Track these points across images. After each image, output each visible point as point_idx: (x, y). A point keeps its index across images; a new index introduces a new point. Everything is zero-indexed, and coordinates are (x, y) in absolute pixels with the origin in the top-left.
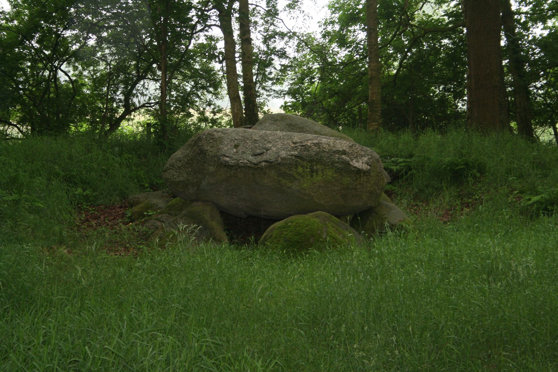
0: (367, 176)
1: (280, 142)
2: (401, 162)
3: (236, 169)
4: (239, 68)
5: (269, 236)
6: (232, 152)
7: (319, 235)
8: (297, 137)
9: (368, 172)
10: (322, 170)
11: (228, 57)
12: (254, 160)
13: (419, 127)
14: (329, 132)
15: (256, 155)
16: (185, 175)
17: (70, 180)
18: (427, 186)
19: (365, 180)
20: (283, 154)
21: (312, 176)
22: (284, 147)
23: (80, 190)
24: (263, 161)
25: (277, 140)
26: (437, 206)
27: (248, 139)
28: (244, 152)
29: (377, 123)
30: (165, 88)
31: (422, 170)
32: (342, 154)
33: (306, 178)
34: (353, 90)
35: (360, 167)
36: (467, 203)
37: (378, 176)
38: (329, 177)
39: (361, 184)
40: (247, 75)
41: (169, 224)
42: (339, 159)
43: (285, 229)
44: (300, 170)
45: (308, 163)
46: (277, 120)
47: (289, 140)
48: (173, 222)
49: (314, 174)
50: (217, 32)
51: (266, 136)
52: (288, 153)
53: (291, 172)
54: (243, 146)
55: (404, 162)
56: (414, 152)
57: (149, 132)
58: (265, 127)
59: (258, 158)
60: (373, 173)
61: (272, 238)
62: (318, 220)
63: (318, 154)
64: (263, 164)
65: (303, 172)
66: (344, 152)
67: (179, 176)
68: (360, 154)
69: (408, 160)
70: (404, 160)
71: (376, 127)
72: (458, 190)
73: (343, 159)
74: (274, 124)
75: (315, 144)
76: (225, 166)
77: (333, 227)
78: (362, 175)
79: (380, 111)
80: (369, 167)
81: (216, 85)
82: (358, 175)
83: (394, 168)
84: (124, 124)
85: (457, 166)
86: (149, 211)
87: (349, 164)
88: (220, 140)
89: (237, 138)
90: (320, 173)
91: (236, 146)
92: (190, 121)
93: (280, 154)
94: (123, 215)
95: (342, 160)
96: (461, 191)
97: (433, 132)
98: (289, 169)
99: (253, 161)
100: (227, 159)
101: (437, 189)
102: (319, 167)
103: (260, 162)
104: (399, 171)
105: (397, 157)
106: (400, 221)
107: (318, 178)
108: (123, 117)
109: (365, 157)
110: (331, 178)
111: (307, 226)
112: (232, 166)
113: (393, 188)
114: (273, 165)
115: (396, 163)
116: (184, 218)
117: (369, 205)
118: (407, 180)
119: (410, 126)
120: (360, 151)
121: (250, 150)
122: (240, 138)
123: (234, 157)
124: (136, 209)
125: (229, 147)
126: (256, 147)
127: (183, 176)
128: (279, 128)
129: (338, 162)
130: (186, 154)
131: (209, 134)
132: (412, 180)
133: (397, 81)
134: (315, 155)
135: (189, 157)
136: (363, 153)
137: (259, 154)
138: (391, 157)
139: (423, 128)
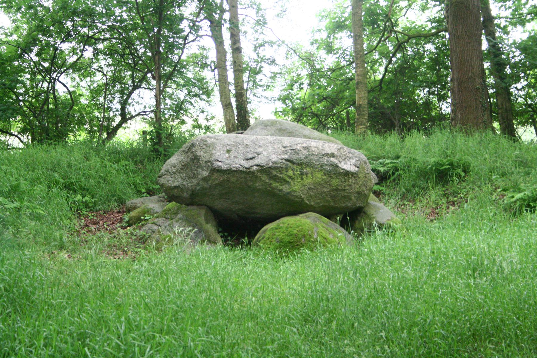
1: (270, 147)
2: (388, 164)
3: (229, 174)
4: (231, 76)
8: (287, 141)
10: (312, 173)
11: (220, 66)
12: (247, 164)
13: (404, 129)
15: (247, 160)
16: (180, 180)
17: (69, 187)
18: (414, 186)
19: (353, 182)
20: (274, 158)
21: (302, 179)
23: (79, 197)
25: (268, 145)
27: (240, 144)
28: (236, 157)
30: (159, 97)
31: (409, 171)
32: (330, 157)
35: (348, 169)
37: (366, 177)
40: (238, 82)
41: (165, 227)
42: (328, 161)
46: (268, 125)
48: (169, 225)
50: (209, 43)
51: (257, 140)
53: (281, 176)
55: (391, 163)
56: (400, 154)
57: (145, 139)
58: (256, 132)
61: (265, 239)
62: (309, 221)
65: (294, 175)
66: (333, 155)
67: (173, 182)
69: (395, 161)
70: (391, 161)
71: (363, 130)
74: (265, 129)
75: (305, 148)
76: (218, 171)
77: (324, 227)
78: (350, 176)
79: (367, 115)
80: (357, 169)
81: (208, 93)
82: (346, 176)
83: (382, 169)
84: (120, 131)
85: (443, 166)
86: (146, 215)
87: (337, 166)
88: (213, 145)
89: (229, 143)
90: (310, 175)
91: (228, 151)
92: (184, 128)
94: (122, 220)
100: (220, 164)
101: (423, 188)
102: (308, 169)
103: (252, 166)
105: (384, 158)
106: (388, 220)
107: (308, 181)
108: (119, 126)
109: (353, 159)
112: (225, 171)
113: (381, 188)
115: (384, 165)
116: (180, 221)
118: (394, 180)
122: (232, 143)
123: (227, 161)
124: (133, 214)
125: (222, 152)
126: (247, 152)
129: (326, 165)
132: (399, 180)
133: (383, 85)
136: (351, 155)
137: (251, 159)
138: (379, 158)
139: (409, 130)
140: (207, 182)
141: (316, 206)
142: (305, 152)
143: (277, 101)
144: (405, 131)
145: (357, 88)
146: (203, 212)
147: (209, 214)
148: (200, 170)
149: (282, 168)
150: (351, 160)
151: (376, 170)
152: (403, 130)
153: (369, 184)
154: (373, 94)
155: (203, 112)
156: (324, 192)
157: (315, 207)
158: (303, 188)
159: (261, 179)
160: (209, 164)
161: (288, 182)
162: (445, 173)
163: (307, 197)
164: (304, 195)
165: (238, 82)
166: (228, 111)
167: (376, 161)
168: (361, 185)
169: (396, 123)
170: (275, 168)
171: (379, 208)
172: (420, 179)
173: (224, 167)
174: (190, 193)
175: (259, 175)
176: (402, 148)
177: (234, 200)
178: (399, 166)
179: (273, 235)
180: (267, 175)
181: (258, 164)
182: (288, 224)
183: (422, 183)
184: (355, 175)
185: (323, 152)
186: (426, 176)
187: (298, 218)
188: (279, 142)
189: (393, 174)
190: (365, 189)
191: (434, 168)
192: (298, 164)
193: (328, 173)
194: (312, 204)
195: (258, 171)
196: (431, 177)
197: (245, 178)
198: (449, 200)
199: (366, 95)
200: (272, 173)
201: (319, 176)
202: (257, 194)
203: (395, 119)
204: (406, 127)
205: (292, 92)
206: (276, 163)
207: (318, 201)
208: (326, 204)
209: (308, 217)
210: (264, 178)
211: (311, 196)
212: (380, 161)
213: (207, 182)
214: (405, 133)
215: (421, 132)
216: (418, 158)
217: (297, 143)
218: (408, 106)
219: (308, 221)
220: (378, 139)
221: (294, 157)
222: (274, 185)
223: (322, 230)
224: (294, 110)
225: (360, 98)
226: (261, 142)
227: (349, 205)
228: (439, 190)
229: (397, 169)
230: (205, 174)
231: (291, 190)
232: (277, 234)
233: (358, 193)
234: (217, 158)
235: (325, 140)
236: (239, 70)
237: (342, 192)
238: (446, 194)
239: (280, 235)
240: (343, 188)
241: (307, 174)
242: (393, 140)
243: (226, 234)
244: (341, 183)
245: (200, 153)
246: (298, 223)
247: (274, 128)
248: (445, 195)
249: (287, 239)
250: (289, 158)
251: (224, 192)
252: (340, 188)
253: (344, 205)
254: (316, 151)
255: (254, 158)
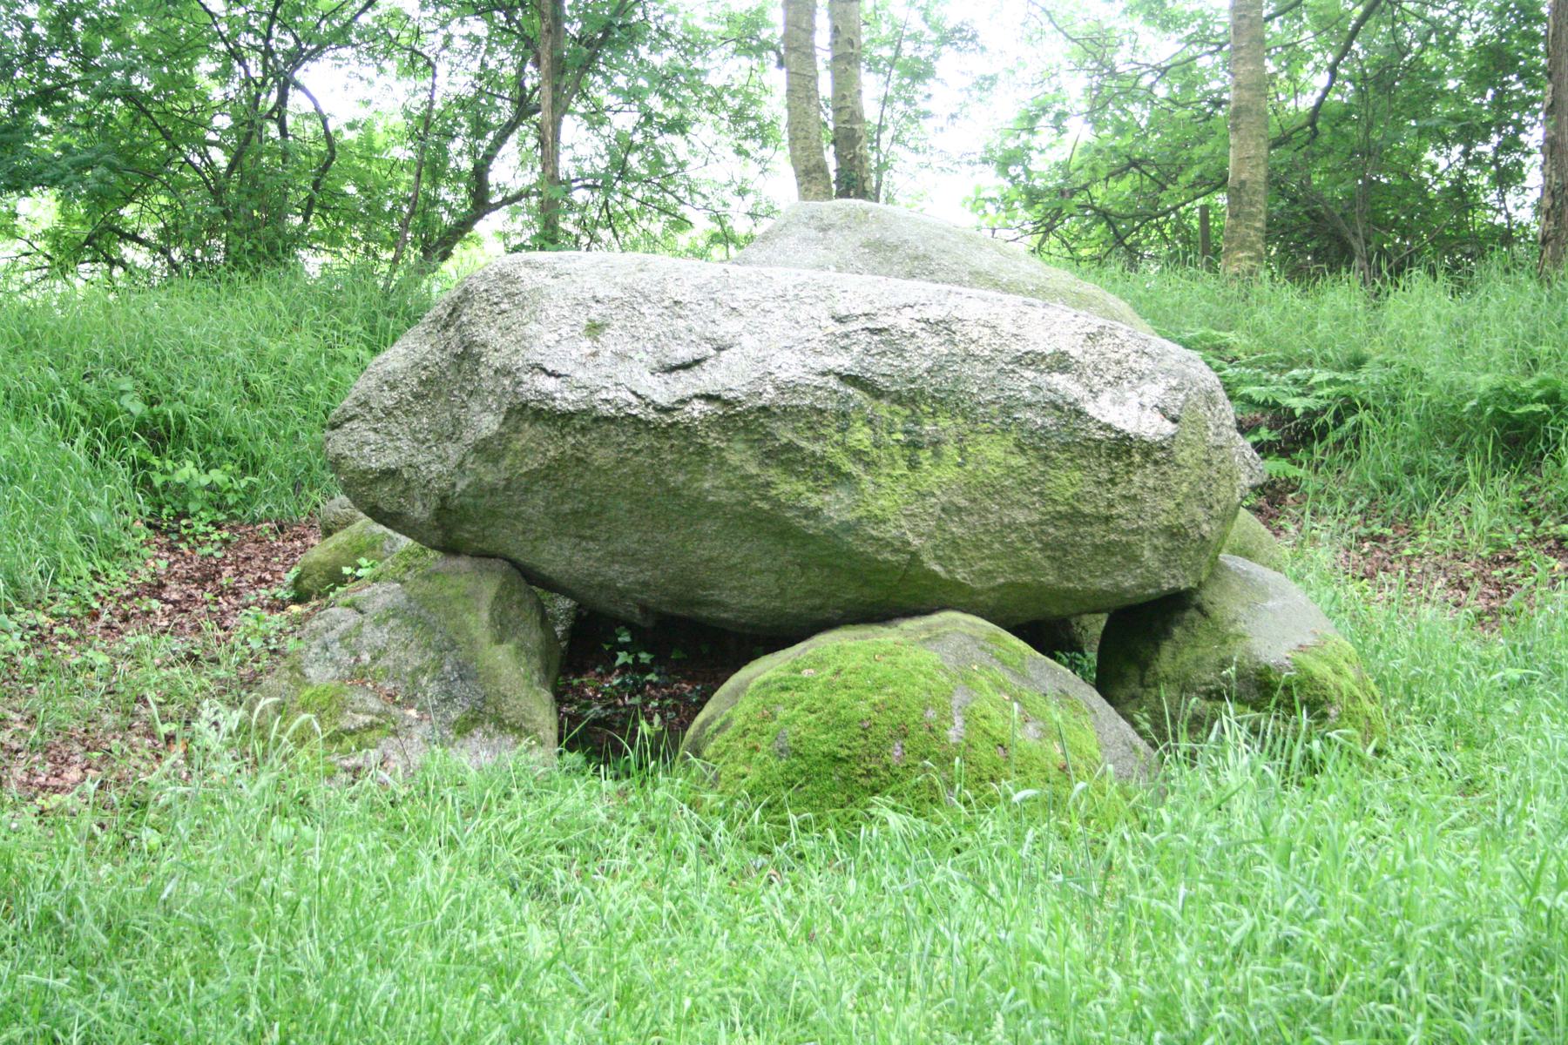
0: (1156, 463)
1: (779, 313)
2: (1320, 385)
3: (584, 430)
5: (717, 723)
6: (575, 354)
7: (931, 730)
9: (1163, 448)
10: (960, 439)
11: (795, 51)
12: (662, 391)
13: (1384, 265)
14: (1032, 276)
16: (405, 444)
18: (1410, 470)
19: (1151, 483)
20: (791, 368)
21: (913, 465)
22: (794, 333)
24: (696, 396)
25: (768, 305)
26: (1446, 543)
27: (647, 298)
28: (622, 356)
29: (1252, 254)
31: (1394, 413)
32: (1050, 369)
33: (886, 471)
34: (1184, 154)
35: (1130, 428)
36: (1555, 537)
37: (1209, 463)
38: (988, 468)
39: (1134, 498)
40: (844, 97)
41: (326, 648)
42: (1036, 389)
43: (786, 695)
44: (860, 436)
45: (896, 407)
47: (821, 305)
48: (341, 639)
49: (925, 455)
52: (809, 362)
53: (817, 448)
54: (623, 327)
55: (1331, 382)
56: (1367, 350)
59: (677, 380)
60: (1186, 453)
61: (729, 733)
62: (935, 657)
63: (942, 367)
64: (699, 407)
65: (876, 445)
66: (1062, 363)
67: (382, 449)
68: (1132, 371)
71: (1246, 265)
72: (1522, 487)
73: (1055, 392)
74: (818, 241)
75: (933, 326)
76: (538, 414)
77: (1000, 688)
78: (1137, 458)
79: (1263, 217)
80: (1169, 428)
82: (1118, 458)
83: (1299, 405)
85: (1521, 403)
86: (363, 561)
87: (1079, 413)
89: (600, 296)
90: (950, 450)
91: (594, 329)
93: (772, 369)
95: (1052, 396)
96: (1532, 490)
97: (1431, 281)
98: (809, 434)
99: (656, 397)
100: (549, 384)
101: (1444, 480)
102: (944, 422)
103: (683, 401)
104: (1309, 414)
105: (1310, 363)
106: (1301, 648)
107: (940, 475)
109: (1153, 381)
110: (998, 472)
111: (878, 686)
112: (567, 416)
113: (1294, 472)
114: (739, 414)
115: (1301, 384)
116: (392, 623)
117: (1165, 587)
118: (1340, 443)
119: (1356, 263)
120: (1133, 356)
121: (650, 348)
122: (616, 293)
123: (579, 374)
125: (565, 330)
127: (397, 448)
128: (834, 257)
129: (1029, 405)
130: (417, 357)
131: (503, 276)
132: (1357, 442)
133: (1319, 125)
134: (929, 371)
135: (425, 368)
136: (1145, 364)
137: (686, 366)
138: (1291, 363)
139: (1398, 270)
140: (496, 462)
141: (978, 586)
142: (932, 344)
143: (979, 167)
144: (1385, 272)
145: (1235, 128)
146: (489, 588)
147: (516, 597)
148: (477, 408)
149: (821, 412)
150: (1146, 387)
151: (1276, 405)
152: (1380, 271)
153: (1223, 492)
154: (1284, 154)
155: (742, 192)
156: (1013, 526)
157: (973, 592)
158: (916, 508)
159: (723, 462)
160: (507, 382)
161: (848, 476)
162: (1526, 430)
163: (935, 547)
164: (920, 535)
165: (844, 97)
166: (814, 189)
167: (1282, 371)
168: (1187, 496)
169: (1357, 245)
170: (788, 413)
171: (1263, 591)
172: (1433, 445)
173: (566, 398)
174: (434, 503)
175: (714, 440)
176: (1375, 329)
177: (618, 546)
178: (1358, 394)
179: (764, 719)
180: (751, 443)
181: (711, 389)
182: (838, 673)
183: (1443, 461)
184: (1159, 455)
185: (1022, 347)
186: (1456, 435)
187: (886, 637)
188: (823, 293)
189: (1339, 419)
190: (1201, 515)
191: (1489, 410)
192: (898, 399)
193: (1034, 444)
194: (961, 575)
195: (710, 424)
196: (1476, 441)
197: (654, 452)
198: (1540, 532)
199: (1263, 151)
200: (771, 435)
201: (994, 452)
202: (709, 527)
203: (1355, 235)
204: (1389, 261)
205: (1035, 142)
206: (794, 388)
207: (987, 565)
208: (1027, 578)
209: (933, 639)
210: (739, 455)
211: (954, 544)
212: (1296, 372)
213: (496, 462)
214: (1384, 282)
215: (1441, 275)
216: (1431, 371)
217: (903, 301)
218: (1397, 195)
219: (929, 657)
220: (1289, 294)
221: (881, 368)
222: (787, 488)
223: (988, 702)
224: (1033, 197)
225: (1241, 160)
226: (741, 295)
227: (1128, 583)
228: (1506, 489)
229: (1351, 408)
230: (488, 424)
231: (861, 512)
232: (783, 713)
233: (1173, 533)
234: (538, 359)
235: (1032, 294)
236: (847, 57)
237: (1098, 529)
238: (1531, 505)
239: (795, 721)
240: (1103, 511)
241: (936, 443)
242: (1343, 303)
243: (645, 657)
244: (1092, 488)
245: (485, 333)
246: (882, 669)
247: (856, 238)
248: (1524, 510)
249: (827, 742)
250: (856, 371)
251: (567, 508)
252: (1087, 509)
253: (1104, 584)
254: (985, 343)
255: (697, 362)
